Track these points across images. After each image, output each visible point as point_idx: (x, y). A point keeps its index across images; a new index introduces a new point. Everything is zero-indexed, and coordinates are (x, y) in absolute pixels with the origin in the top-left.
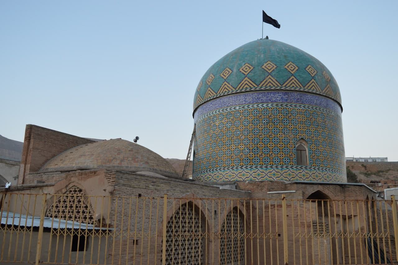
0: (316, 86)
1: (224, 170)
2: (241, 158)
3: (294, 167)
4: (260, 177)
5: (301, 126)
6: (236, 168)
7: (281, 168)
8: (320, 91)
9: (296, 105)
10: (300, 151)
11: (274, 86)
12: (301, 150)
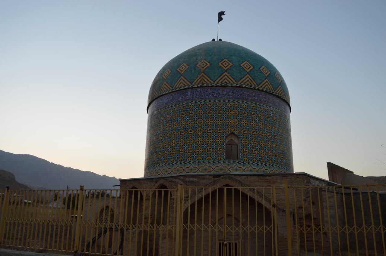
0: (229, 79)
1: (229, 163)
2: (208, 152)
6: (184, 163)
8: (270, 90)
9: (238, 101)
12: (231, 145)
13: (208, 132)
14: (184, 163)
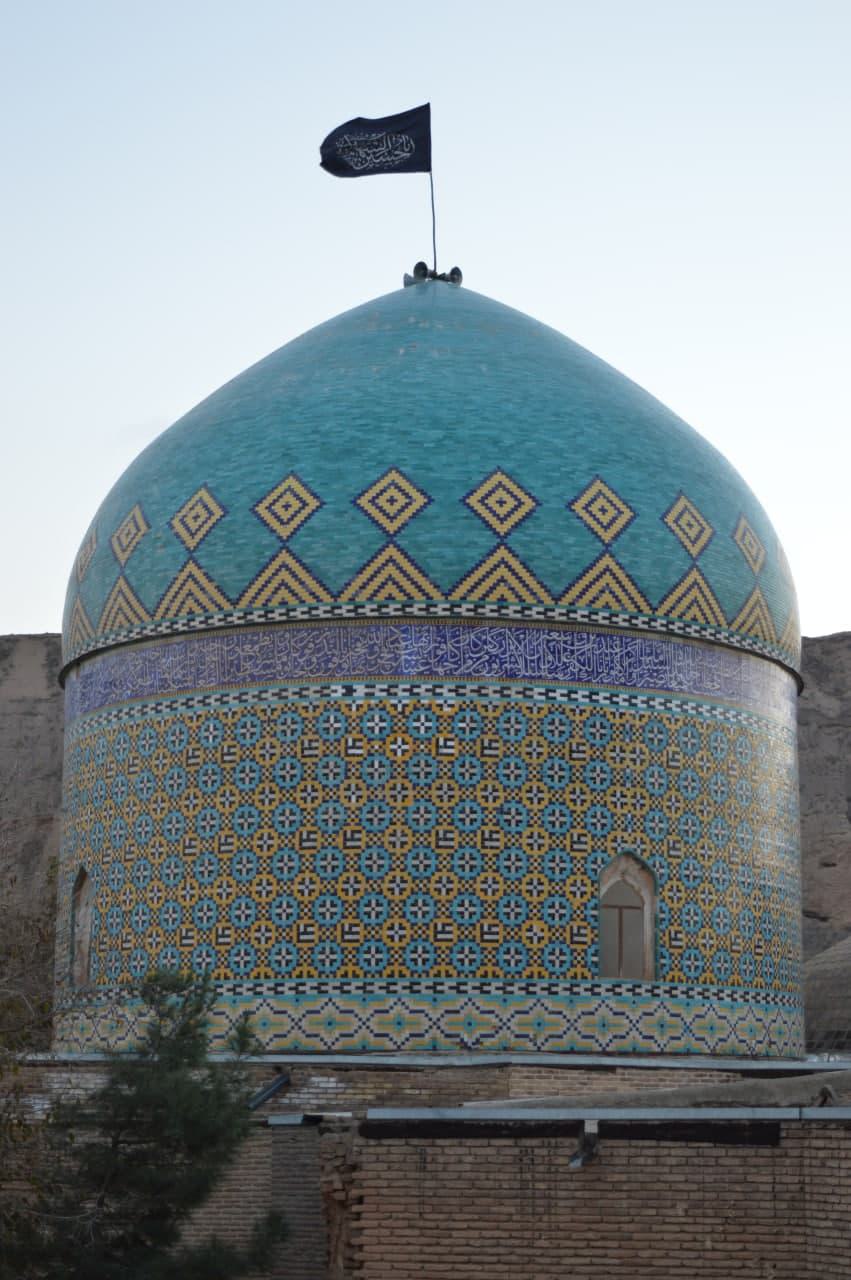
2: (221, 944)
3: (351, 988)
4: (406, 1034)
5: (625, 796)
7: (501, 992)
9: (323, 688)
10: (617, 911)
11: (540, 602)
12: (621, 908)
13: (220, 852)
14: (431, 991)
